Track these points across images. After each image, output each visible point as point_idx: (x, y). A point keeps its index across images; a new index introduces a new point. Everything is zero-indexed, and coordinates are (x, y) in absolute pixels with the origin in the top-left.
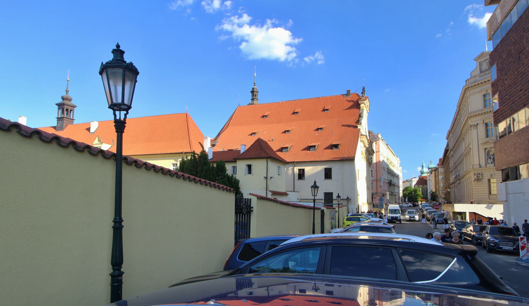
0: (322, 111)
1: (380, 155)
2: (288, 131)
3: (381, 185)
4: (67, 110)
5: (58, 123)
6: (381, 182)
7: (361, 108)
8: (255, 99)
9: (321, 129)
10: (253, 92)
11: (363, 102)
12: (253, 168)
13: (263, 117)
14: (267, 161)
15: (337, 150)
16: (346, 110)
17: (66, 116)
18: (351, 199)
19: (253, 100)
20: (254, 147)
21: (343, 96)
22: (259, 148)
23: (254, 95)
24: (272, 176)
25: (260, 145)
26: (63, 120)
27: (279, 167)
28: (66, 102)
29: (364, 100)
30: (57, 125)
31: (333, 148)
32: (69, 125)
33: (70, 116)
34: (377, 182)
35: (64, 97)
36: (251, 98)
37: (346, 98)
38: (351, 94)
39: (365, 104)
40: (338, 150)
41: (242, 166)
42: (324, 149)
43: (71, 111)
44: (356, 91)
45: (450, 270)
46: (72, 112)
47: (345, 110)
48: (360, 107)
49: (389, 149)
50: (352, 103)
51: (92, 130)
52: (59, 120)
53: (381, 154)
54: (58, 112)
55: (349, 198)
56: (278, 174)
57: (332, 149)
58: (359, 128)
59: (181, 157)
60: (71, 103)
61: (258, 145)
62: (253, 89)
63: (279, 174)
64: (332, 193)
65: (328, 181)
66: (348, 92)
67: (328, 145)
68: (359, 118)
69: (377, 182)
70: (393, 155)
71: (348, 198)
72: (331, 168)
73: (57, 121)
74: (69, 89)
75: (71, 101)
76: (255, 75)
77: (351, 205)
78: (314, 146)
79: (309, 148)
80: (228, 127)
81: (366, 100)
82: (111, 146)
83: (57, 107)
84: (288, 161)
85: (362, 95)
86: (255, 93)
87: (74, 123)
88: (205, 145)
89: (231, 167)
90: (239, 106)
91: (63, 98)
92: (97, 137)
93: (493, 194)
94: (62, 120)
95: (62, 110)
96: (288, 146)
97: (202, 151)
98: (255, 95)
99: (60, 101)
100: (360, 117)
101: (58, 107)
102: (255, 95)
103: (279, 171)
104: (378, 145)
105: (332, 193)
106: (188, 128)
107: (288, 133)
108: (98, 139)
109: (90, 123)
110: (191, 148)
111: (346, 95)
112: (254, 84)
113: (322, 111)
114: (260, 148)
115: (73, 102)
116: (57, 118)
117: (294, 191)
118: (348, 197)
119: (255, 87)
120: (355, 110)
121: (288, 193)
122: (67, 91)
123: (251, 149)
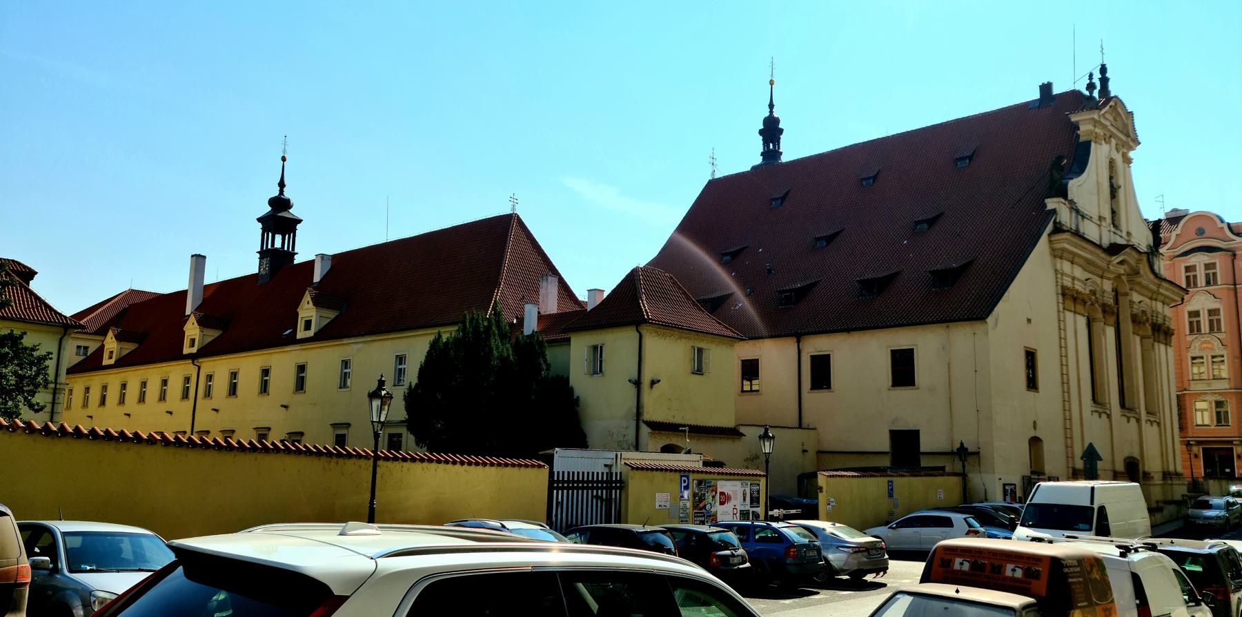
24: (656, 378)
45: (27, 540)
65: (904, 393)
72: (912, 350)
77: (980, 473)
84: (638, 335)
88: (543, 297)
93: (1199, 422)
115: (295, 212)
117: (800, 427)
121: (742, 430)
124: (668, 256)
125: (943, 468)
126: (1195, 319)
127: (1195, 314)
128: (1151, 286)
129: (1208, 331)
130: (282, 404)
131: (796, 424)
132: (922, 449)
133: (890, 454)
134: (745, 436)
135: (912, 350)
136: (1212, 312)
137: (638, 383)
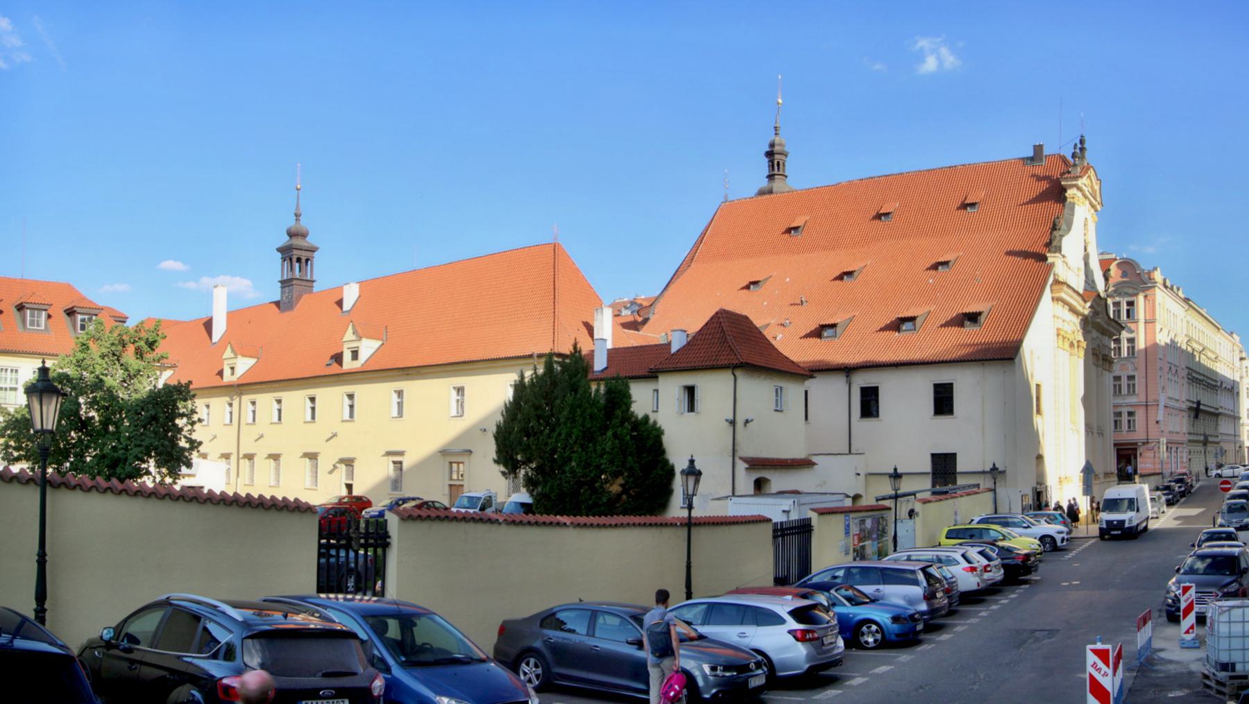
0: (958, 209)
1: (1158, 330)
2: (850, 274)
3: (1158, 419)
4: (299, 260)
5: (282, 293)
6: (1158, 409)
7: (1068, 200)
8: (776, 177)
9: (946, 263)
10: (770, 154)
11: (1074, 183)
12: (698, 394)
13: (789, 231)
14: (735, 376)
15: (975, 329)
16: (1022, 205)
17: (297, 274)
18: (1007, 472)
19: (771, 177)
20: (706, 334)
21: (1021, 162)
22: (718, 336)
23: (776, 163)
25: (722, 329)
26: (292, 285)
27: (777, 390)
28: (297, 242)
29: (1076, 178)
30: (282, 297)
31: (966, 322)
32: (303, 297)
33: (306, 275)
34: (1147, 410)
35: (292, 231)
36: (767, 173)
37: (1030, 169)
38: (1046, 156)
39: (1079, 189)
40: (978, 328)
41: (671, 388)
42: (941, 326)
43: (307, 260)
44: (1060, 148)
46: (309, 262)
47: (1020, 205)
48: (1065, 199)
49: (1194, 311)
50: (1044, 185)
51: (347, 305)
52: (285, 287)
53: (1161, 329)
54: (283, 265)
55: (997, 469)
56: (776, 410)
57: (962, 325)
58: (1050, 260)
59: (532, 367)
60: (307, 242)
61: (715, 328)
62: (772, 145)
63: (779, 408)
64: (933, 455)
65: (944, 420)
66: (1038, 149)
67: (955, 315)
68: (1051, 233)
69: (1147, 410)
70: (1212, 326)
71: (994, 469)
72: (952, 384)
73: (282, 288)
74: (302, 211)
75: (306, 237)
76: (780, 101)
78: (912, 319)
79: (897, 325)
80: (689, 266)
81: (1080, 177)
82: (381, 343)
83: (279, 255)
85: (1075, 161)
86: (777, 157)
87: (315, 289)
89: (652, 391)
90: (726, 201)
91: (291, 234)
92: (351, 324)
94: (289, 286)
95: (289, 261)
96: (838, 321)
97: (573, 351)
98: (778, 162)
99: (284, 240)
100: (1056, 229)
101: (282, 254)
102: (778, 162)
103: (777, 400)
104: (1151, 302)
105: (933, 455)
106: (554, 285)
107: (850, 280)
108: (353, 329)
109: (341, 289)
110: (554, 341)
111: (1032, 159)
112: (776, 130)
113: (958, 209)
114: (719, 338)
115: (311, 240)
116: (280, 282)
118: (994, 465)
119: (777, 140)
120: (1051, 207)
121: (814, 459)
122: (297, 216)
123: (698, 343)
124: (1123, 676)
125: (978, 486)
126: (1117, 383)
127: (1117, 378)
128: (458, 692)
129: (1126, 393)
130: (254, 440)
131: (847, 452)
132: (959, 469)
133: (930, 476)
134: (817, 464)
135: (952, 384)
136: (1131, 378)
137: (733, 423)
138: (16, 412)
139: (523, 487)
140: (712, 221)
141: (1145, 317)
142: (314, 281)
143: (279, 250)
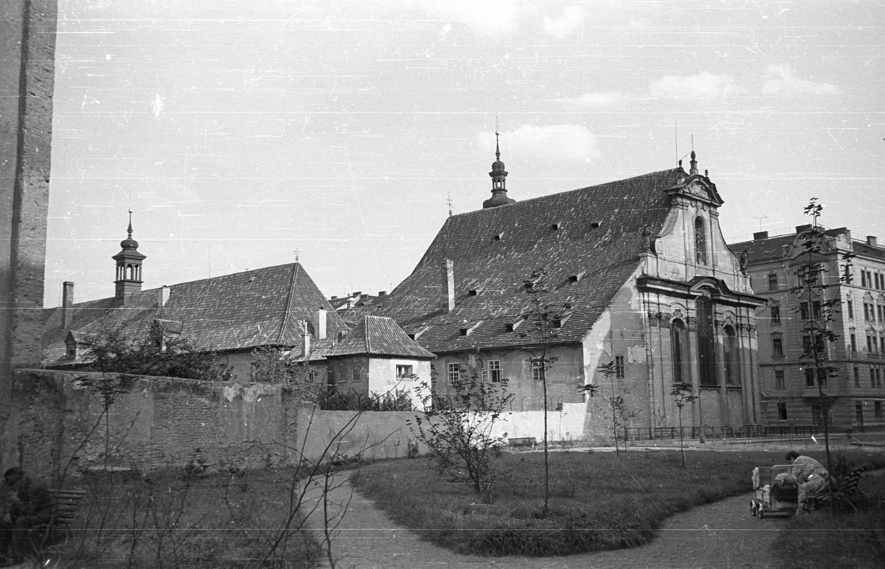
43: (137, 266)
46: (138, 267)
83: (115, 262)
122: (130, 230)
134: (145, 257)
138: (214, 393)
139: (700, 491)
140: (546, 434)
141: (724, 350)
142: (141, 282)
143: (114, 258)
